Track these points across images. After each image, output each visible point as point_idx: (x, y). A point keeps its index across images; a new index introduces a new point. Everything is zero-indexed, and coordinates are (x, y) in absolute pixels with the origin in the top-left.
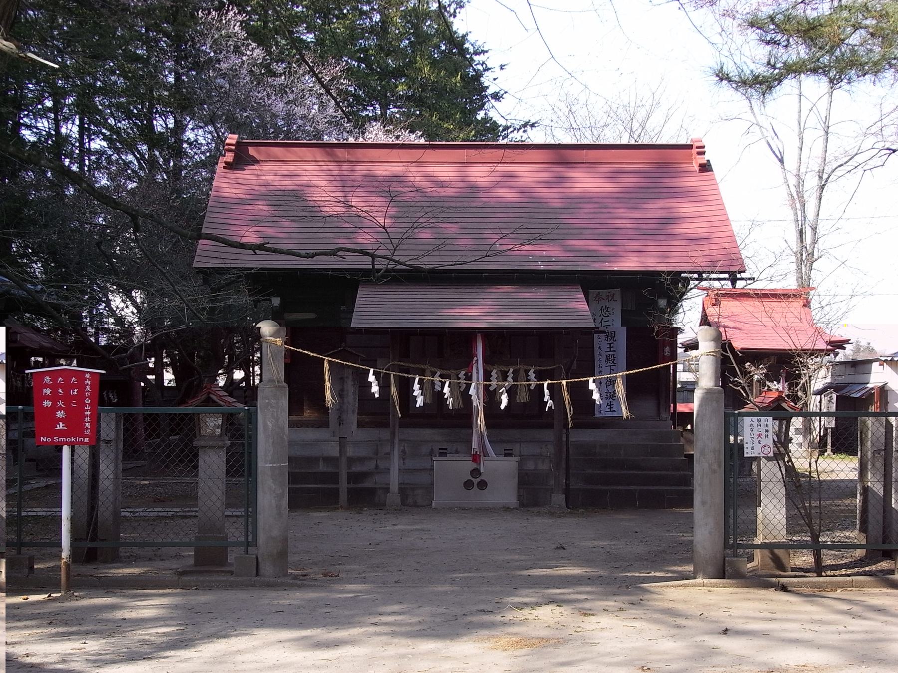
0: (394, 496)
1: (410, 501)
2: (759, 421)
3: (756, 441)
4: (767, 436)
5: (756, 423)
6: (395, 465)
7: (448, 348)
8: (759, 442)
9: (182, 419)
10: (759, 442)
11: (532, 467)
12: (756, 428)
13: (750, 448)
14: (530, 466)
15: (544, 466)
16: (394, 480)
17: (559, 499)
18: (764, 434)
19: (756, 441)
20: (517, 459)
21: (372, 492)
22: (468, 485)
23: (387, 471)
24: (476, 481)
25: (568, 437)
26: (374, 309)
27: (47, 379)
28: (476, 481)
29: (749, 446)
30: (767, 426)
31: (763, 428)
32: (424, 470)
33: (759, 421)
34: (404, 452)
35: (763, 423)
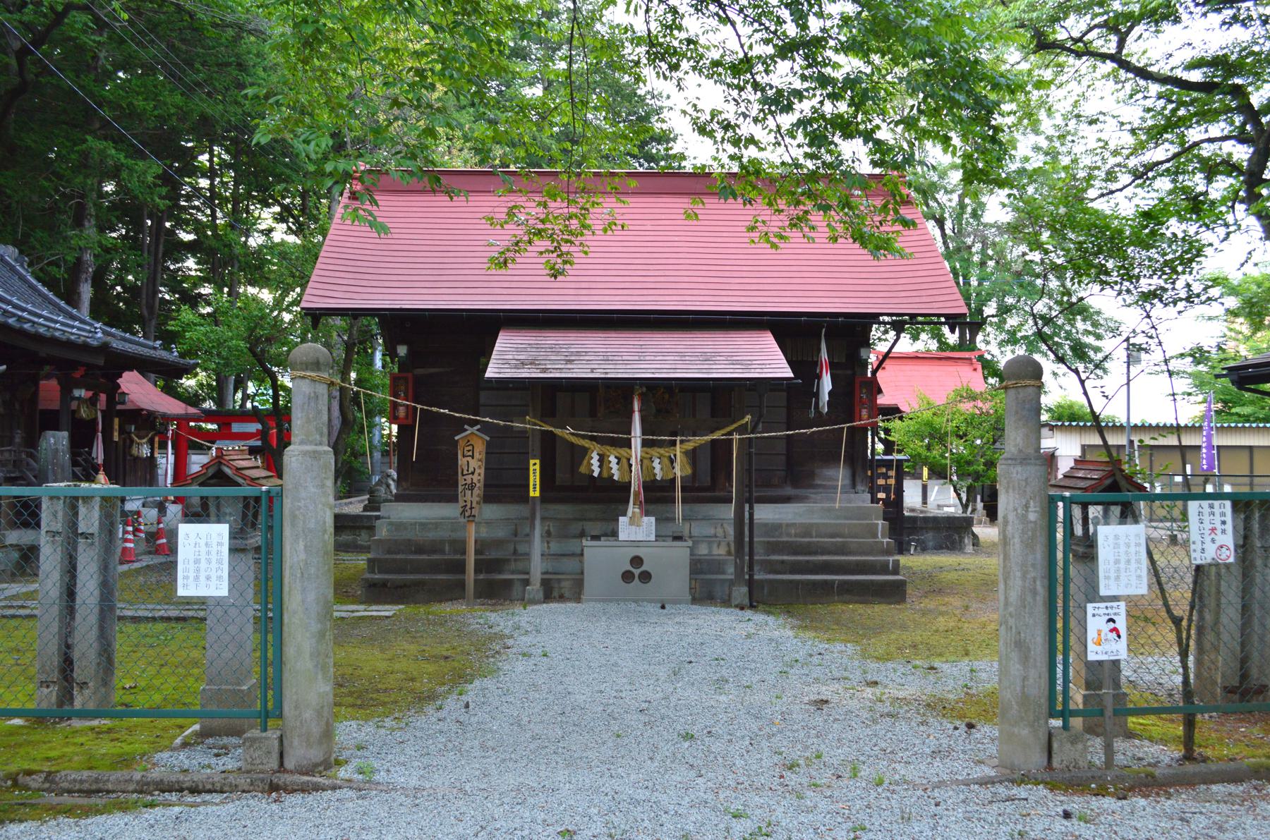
0: (535, 588)
1: (556, 594)
2: (1211, 507)
3: (1208, 539)
4: (1224, 532)
5: (1206, 510)
6: (537, 546)
7: (604, 401)
8: (1213, 541)
9: (1136, 618)
10: (1213, 541)
11: (705, 552)
12: (1206, 518)
13: (1199, 550)
14: (703, 550)
15: (720, 551)
16: (537, 567)
17: (741, 592)
18: (1219, 527)
19: (1208, 539)
20: (690, 543)
21: (508, 584)
22: (627, 577)
23: (527, 556)
24: (637, 572)
25: (751, 515)
26: (509, 357)
27: (1063, 335)
28: (637, 572)
29: (1198, 547)
30: (1223, 514)
31: (1218, 519)
32: (573, 555)
33: (1211, 507)
34: (549, 533)
35: (1217, 510)
